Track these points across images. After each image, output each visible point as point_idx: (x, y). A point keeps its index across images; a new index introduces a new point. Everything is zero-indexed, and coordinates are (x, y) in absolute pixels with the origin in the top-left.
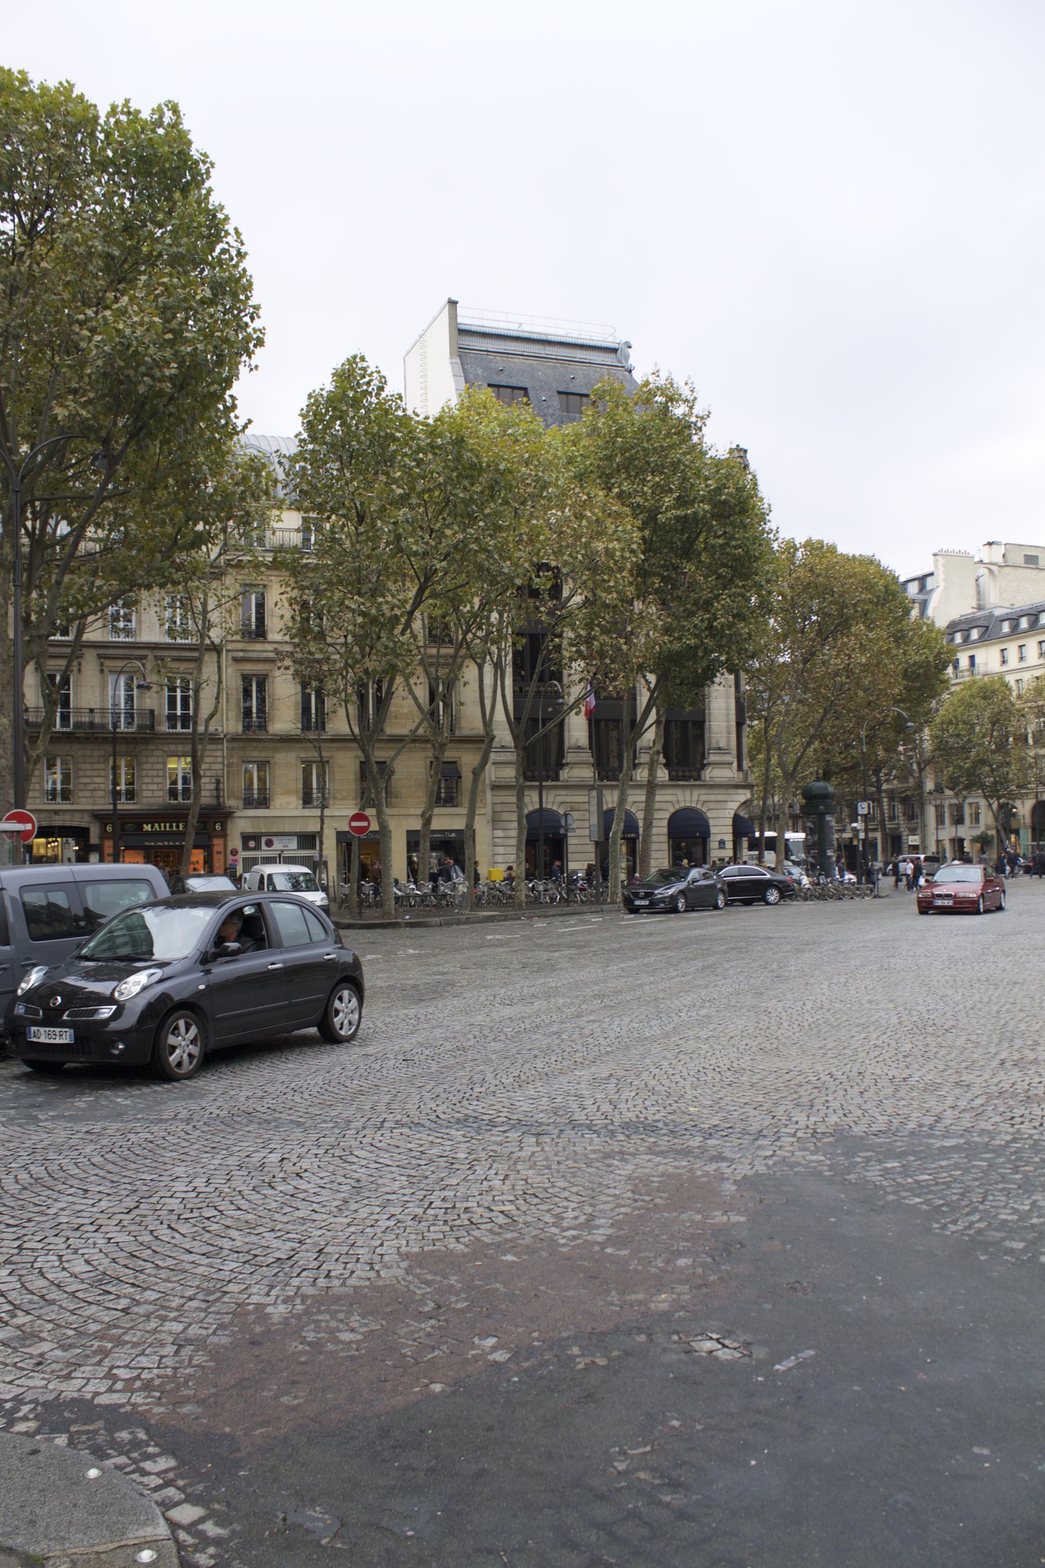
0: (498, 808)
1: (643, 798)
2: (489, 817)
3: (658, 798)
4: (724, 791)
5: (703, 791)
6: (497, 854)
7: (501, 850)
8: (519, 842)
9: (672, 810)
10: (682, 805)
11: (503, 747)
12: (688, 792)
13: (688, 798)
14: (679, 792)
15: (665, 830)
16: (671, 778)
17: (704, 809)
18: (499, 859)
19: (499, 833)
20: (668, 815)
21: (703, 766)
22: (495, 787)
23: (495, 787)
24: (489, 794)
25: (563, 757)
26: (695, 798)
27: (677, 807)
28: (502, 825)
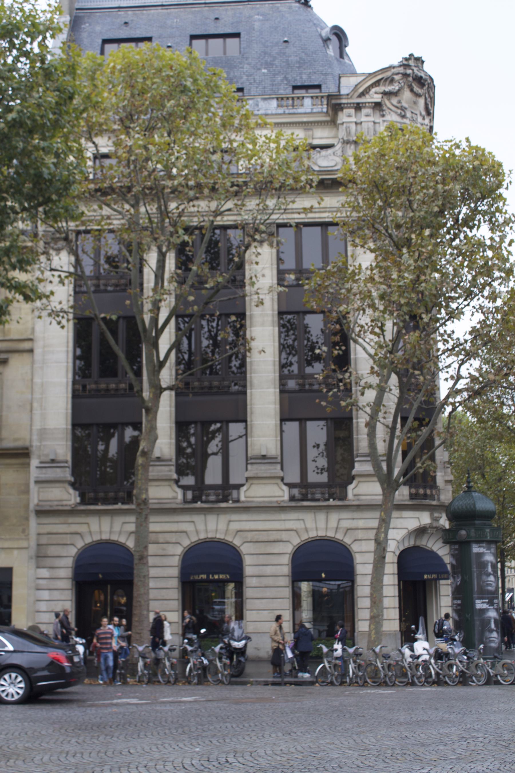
0: (44, 540)
1: (375, 524)
2: (33, 551)
3: (153, 527)
4: (61, 519)
5: (345, 515)
6: (266, 612)
7: (45, 595)
8: (146, 585)
9: (296, 541)
10: (313, 534)
11: (264, 457)
12: (321, 517)
13: (321, 524)
14: (199, 519)
15: (175, 572)
16: (83, 501)
17: (347, 540)
18: (43, 606)
19: (44, 573)
20: (289, 549)
21: (351, 479)
22: (40, 513)
23: (40, 513)
24: (33, 521)
25: (353, 467)
26: (117, 527)
27: (305, 537)
28: (48, 562)
